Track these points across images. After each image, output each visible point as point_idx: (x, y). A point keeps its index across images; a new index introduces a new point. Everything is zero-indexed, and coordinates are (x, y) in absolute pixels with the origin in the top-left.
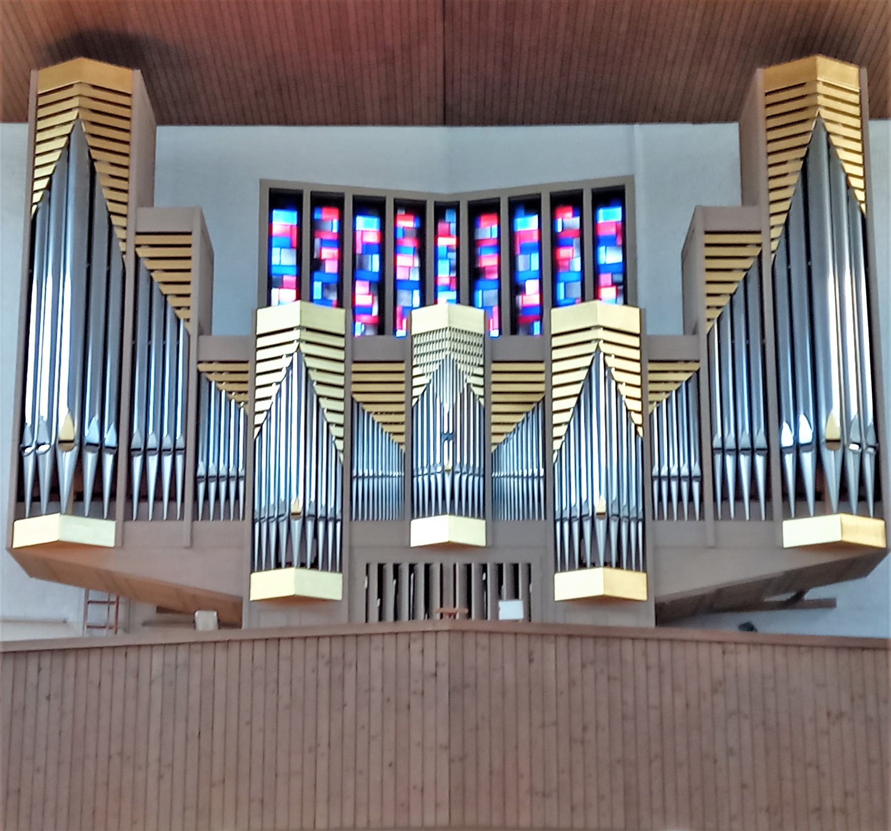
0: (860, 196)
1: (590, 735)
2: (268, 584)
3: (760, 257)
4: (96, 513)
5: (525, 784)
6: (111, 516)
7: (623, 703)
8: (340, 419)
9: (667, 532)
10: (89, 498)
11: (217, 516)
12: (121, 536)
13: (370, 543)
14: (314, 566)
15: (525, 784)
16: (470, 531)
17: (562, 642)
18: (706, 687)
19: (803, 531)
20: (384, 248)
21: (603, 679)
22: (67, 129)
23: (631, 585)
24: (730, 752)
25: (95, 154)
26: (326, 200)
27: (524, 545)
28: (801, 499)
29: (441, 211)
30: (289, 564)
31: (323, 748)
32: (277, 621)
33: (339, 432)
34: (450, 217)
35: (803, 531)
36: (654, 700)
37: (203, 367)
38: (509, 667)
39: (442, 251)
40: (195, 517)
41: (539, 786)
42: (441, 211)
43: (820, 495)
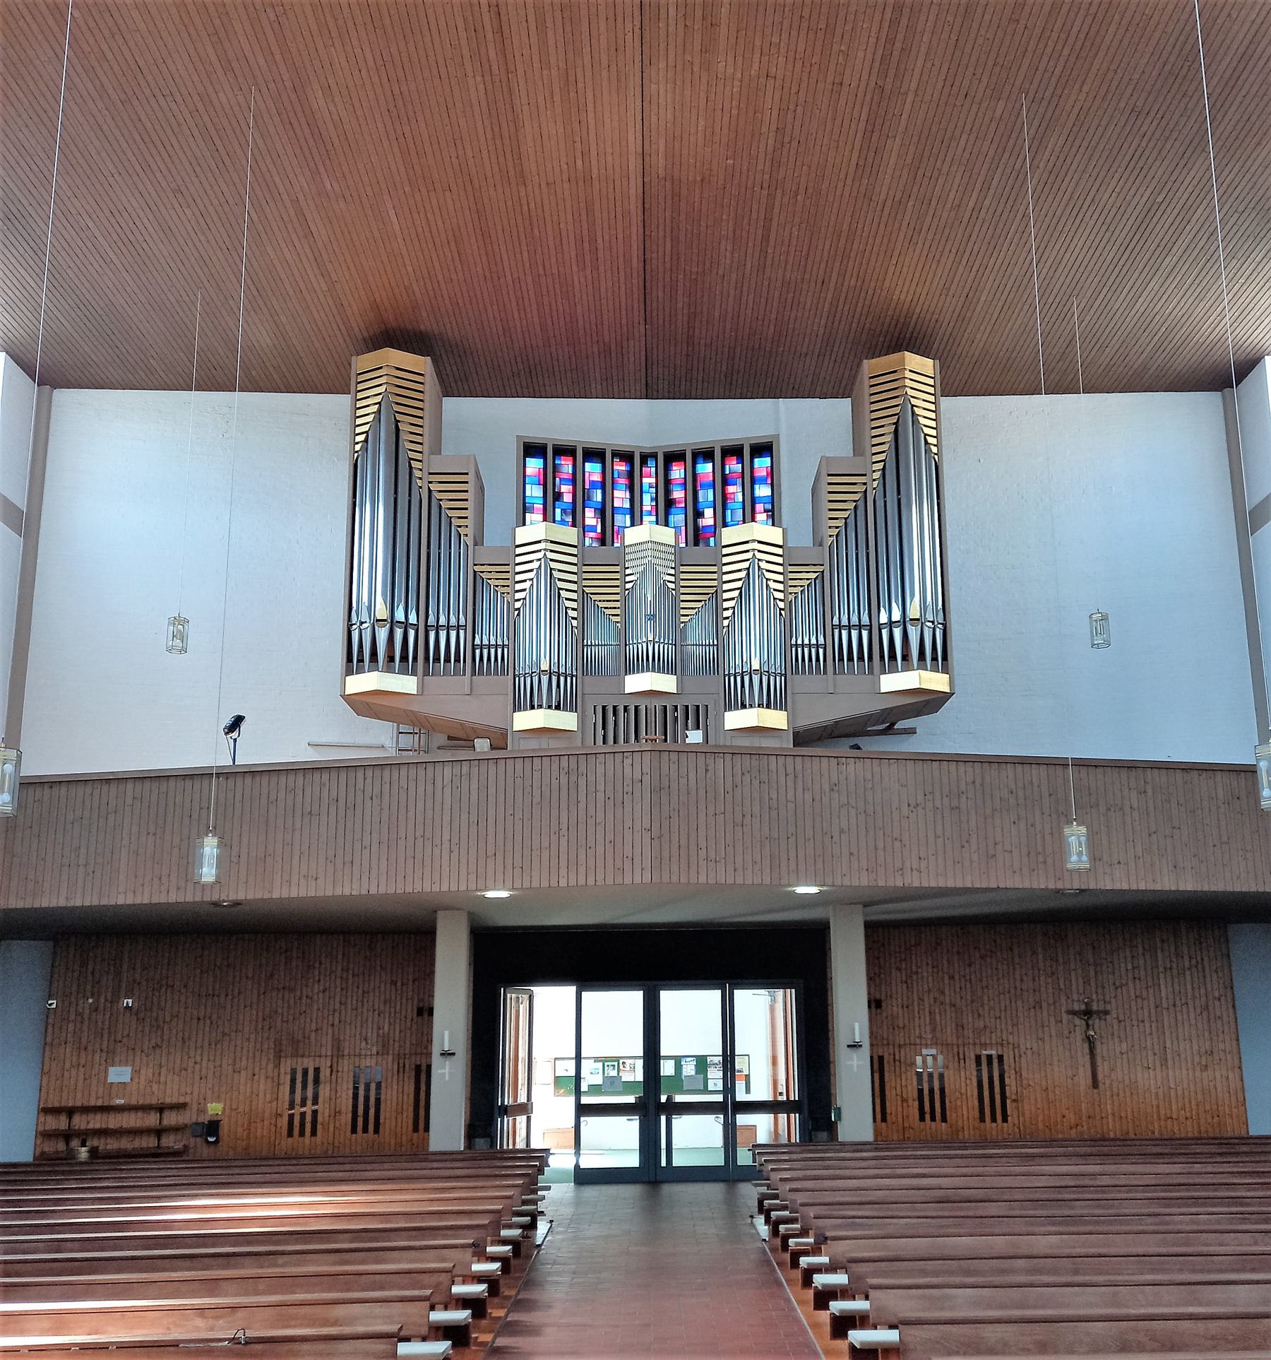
0: (934, 450)
1: (747, 820)
2: (524, 720)
3: (865, 492)
4: (404, 671)
5: (703, 853)
6: (414, 673)
7: (770, 799)
8: (574, 605)
9: (801, 683)
10: (399, 660)
11: (489, 673)
12: (421, 686)
13: (596, 692)
14: (558, 708)
15: (703, 853)
16: (667, 683)
17: (728, 757)
18: (826, 787)
19: (893, 682)
20: (605, 485)
21: (756, 783)
22: (378, 399)
23: (776, 719)
24: (842, 831)
25: (399, 417)
26: (561, 451)
27: (706, 690)
28: (891, 660)
29: (644, 459)
30: (540, 706)
31: (564, 831)
32: (532, 744)
33: (574, 614)
34: (651, 463)
35: (893, 682)
36: (790, 796)
37: (476, 568)
38: (692, 775)
39: (645, 487)
40: (473, 673)
41: (712, 855)
42: (644, 459)
43: (905, 657)
